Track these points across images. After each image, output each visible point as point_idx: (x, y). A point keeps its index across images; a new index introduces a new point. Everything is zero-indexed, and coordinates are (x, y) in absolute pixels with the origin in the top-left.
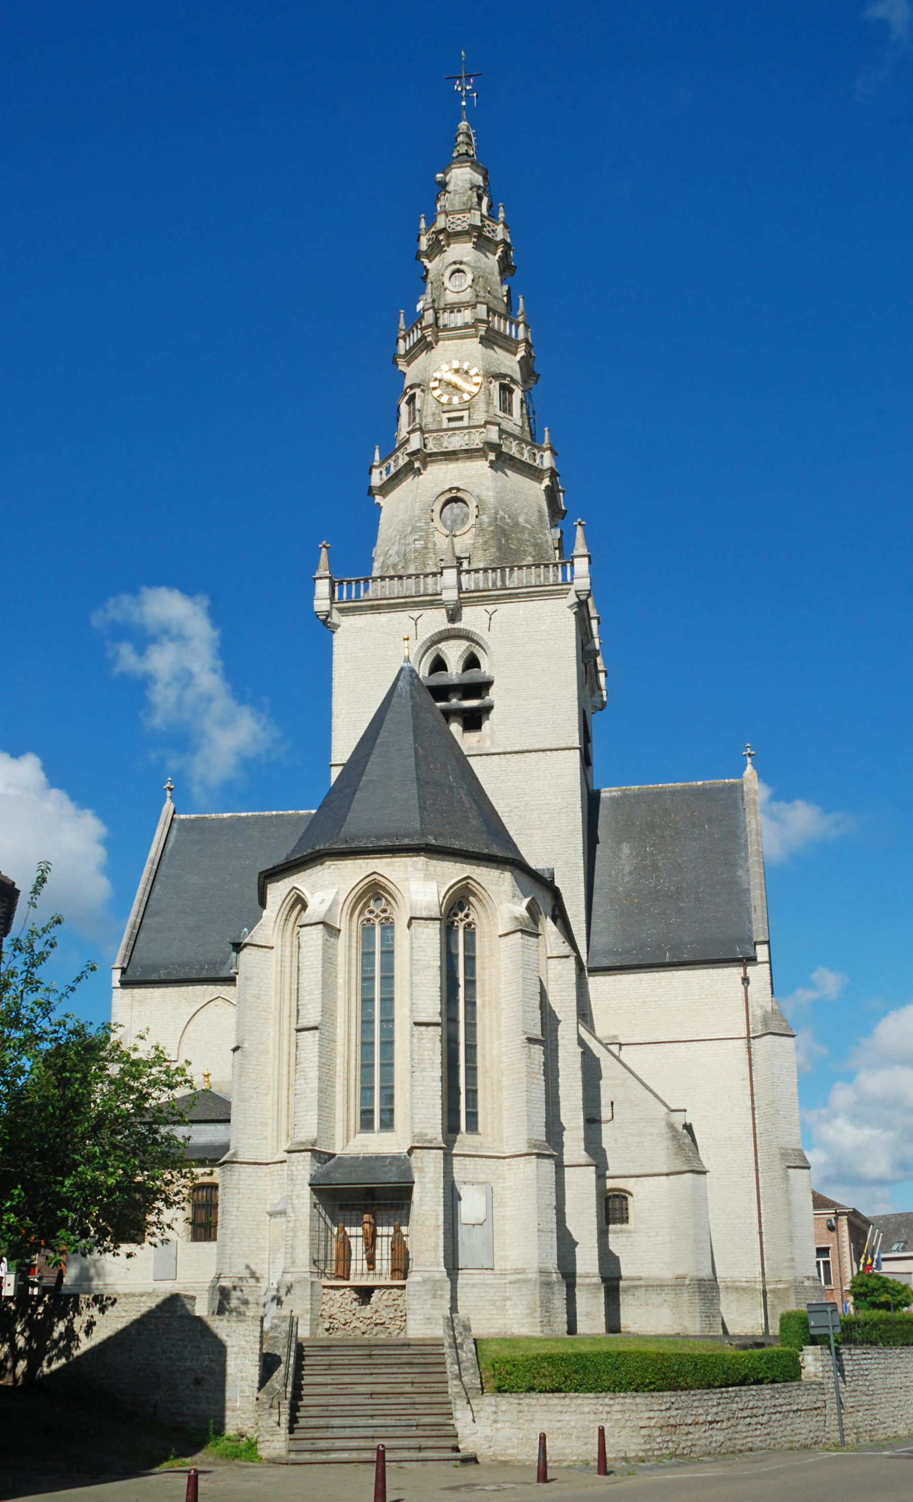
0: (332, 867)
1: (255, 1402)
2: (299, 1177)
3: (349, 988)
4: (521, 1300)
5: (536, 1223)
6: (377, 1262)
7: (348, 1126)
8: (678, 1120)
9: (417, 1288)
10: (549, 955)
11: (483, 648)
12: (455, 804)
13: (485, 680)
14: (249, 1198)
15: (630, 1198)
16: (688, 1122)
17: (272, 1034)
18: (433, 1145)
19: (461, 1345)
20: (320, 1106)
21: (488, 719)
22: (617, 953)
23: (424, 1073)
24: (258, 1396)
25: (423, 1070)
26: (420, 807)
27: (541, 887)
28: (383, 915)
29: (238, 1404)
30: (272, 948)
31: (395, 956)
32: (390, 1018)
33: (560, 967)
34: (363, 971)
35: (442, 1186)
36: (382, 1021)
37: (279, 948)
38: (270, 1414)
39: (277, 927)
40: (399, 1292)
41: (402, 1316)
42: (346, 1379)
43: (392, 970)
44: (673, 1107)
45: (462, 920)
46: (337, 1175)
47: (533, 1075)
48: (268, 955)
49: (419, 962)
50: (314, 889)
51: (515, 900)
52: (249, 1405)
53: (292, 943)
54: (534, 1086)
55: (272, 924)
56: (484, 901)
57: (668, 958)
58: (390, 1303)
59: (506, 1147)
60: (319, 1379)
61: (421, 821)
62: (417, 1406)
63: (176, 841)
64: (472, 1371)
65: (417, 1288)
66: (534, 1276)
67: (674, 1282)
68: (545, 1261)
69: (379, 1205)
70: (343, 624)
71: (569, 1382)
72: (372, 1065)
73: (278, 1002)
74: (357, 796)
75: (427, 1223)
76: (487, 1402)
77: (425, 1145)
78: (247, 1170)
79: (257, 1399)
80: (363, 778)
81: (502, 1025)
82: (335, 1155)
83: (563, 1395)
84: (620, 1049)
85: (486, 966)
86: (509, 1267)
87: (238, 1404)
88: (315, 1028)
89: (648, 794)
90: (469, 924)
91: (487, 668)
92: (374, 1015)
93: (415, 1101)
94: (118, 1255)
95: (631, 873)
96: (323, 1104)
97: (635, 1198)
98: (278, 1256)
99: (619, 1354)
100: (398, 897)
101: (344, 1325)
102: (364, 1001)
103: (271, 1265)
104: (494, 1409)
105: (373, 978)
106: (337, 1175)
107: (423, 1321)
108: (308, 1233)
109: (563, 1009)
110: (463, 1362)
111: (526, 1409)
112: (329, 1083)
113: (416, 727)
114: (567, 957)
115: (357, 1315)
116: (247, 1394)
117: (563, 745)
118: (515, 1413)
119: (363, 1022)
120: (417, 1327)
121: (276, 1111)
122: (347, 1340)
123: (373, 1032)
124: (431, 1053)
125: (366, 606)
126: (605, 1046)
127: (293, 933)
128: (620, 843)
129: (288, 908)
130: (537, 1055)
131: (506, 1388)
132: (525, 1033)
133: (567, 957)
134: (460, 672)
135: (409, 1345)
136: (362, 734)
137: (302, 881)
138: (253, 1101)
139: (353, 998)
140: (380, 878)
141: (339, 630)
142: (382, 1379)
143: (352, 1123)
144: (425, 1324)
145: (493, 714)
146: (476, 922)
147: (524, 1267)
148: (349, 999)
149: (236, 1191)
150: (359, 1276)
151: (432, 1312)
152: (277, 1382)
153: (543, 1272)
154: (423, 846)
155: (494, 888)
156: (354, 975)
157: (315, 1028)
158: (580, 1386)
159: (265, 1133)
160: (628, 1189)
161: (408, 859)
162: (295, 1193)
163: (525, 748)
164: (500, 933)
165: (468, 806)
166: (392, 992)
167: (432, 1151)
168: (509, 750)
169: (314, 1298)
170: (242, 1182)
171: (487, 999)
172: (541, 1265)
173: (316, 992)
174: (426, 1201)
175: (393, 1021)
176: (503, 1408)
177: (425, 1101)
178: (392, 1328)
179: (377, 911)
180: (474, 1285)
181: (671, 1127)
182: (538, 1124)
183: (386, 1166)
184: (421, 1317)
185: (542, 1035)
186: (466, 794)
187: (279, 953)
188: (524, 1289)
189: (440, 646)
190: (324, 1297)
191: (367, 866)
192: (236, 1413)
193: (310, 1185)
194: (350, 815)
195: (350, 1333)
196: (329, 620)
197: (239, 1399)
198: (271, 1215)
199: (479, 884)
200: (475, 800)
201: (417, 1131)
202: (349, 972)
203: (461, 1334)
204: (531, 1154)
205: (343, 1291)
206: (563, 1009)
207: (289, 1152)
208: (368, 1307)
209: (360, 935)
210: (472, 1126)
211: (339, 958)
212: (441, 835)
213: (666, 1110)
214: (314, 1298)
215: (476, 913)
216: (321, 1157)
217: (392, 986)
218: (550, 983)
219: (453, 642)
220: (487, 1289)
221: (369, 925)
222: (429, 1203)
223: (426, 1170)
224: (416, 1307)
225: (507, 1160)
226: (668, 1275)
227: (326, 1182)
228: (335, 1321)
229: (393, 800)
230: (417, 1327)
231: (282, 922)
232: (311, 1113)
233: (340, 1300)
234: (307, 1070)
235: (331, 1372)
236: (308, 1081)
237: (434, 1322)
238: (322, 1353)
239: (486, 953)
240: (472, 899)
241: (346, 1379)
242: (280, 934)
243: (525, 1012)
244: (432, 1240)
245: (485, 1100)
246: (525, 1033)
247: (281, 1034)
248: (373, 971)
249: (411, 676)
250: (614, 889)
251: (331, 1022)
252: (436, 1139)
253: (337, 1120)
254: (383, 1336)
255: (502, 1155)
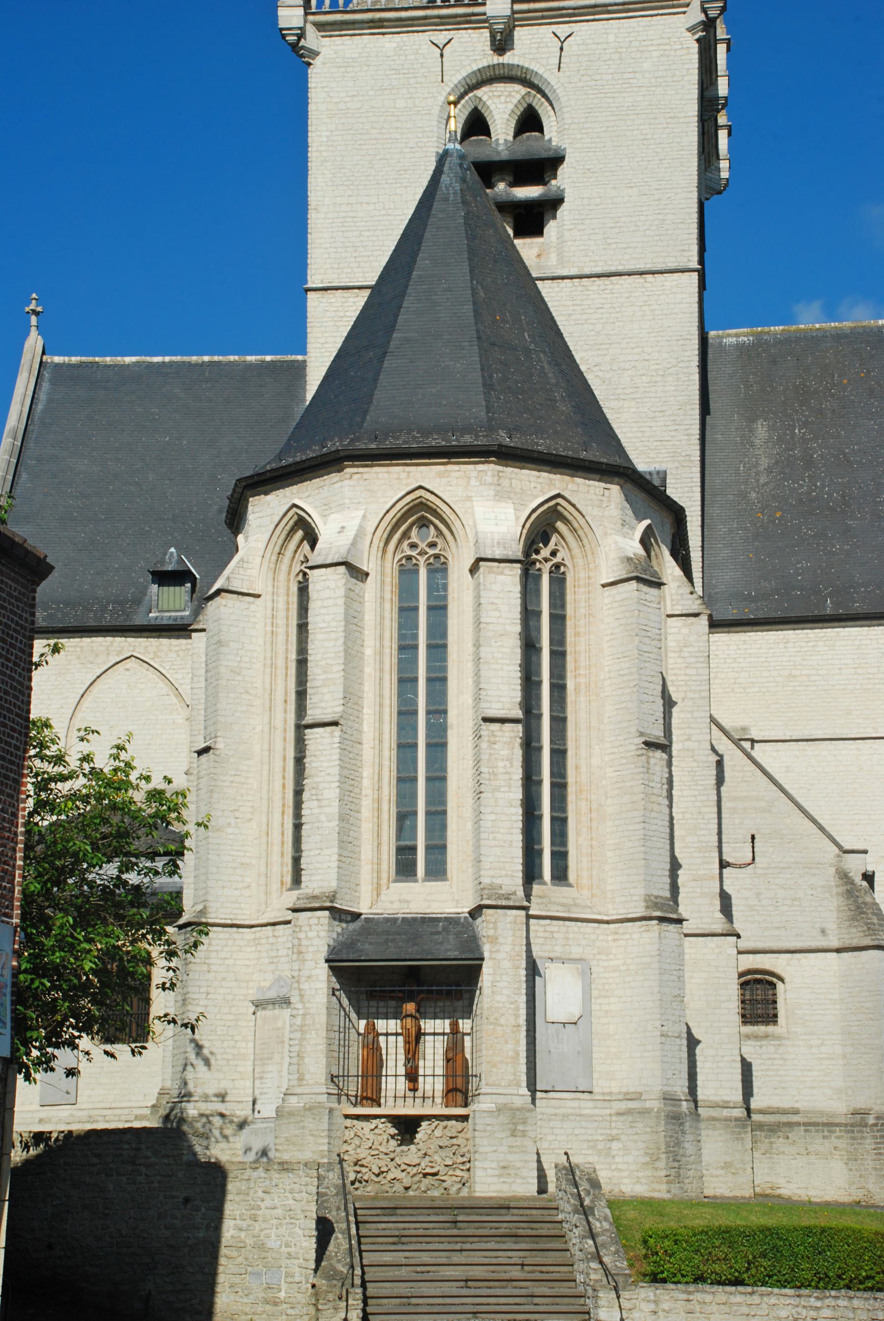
0: (356, 477)
1: (310, 1290)
2: (311, 949)
3: (381, 662)
4: (636, 1141)
5: (658, 1024)
6: (421, 1079)
7: (379, 872)
8: (855, 866)
9: (489, 1121)
10: (669, 613)
11: (551, 105)
12: (535, 379)
13: (551, 154)
14: (224, 979)
15: (779, 985)
16: (870, 869)
17: (259, 729)
18: (511, 903)
19: (592, 1209)
20: (341, 841)
21: (554, 217)
22: (749, 598)
23: (499, 795)
24: (315, 1282)
25: (497, 789)
26: (484, 385)
27: (647, 492)
28: (431, 552)
29: (282, 1295)
30: (259, 596)
31: (450, 615)
32: (442, 708)
33: (685, 631)
34: (401, 637)
35: (524, 965)
36: (428, 712)
37: (269, 598)
38: (336, 1309)
39: (266, 564)
40: (459, 1125)
41: (463, 1163)
42: (426, 1258)
43: (444, 635)
44: (847, 847)
45: (546, 560)
46: (367, 946)
47: (653, 798)
48: (253, 607)
49: (491, 627)
50: (327, 509)
51: (625, 529)
52: (299, 1296)
53: (288, 588)
54: (653, 815)
55: (260, 559)
56: (580, 532)
57: (829, 608)
58: (444, 1142)
59: (610, 906)
60: (387, 1258)
61: (487, 407)
62: (536, 1300)
63: (50, 400)
64: (613, 1249)
65: (489, 1121)
66: (655, 1105)
67: (849, 1120)
68: (670, 1081)
69: (430, 992)
70: (324, 51)
71: (753, 1271)
72: (415, 779)
73: (268, 680)
74: (386, 364)
75: (503, 1021)
76: (643, 1296)
77: (499, 903)
78: (221, 936)
79: (313, 1286)
80: (394, 335)
81: (606, 721)
82: (361, 914)
83: (749, 1289)
84: (752, 748)
85: (582, 630)
86: (615, 1090)
87: (282, 1295)
88: (335, 724)
89: (798, 340)
90: (557, 566)
91: (554, 132)
92: (416, 704)
93: (483, 836)
94: (52, 1070)
95: (769, 470)
96: (345, 838)
97: (788, 985)
98: (269, 1068)
99: (823, 1230)
100: (456, 526)
101: (378, 1175)
102: (401, 681)
103: (257, 1083)
104: (652, 1307)
105: (416, 647)
106: (367, 946)
107: (498, 1172)
108: (324, 1034)
109: (690, 695)
110: (598, 1235)
111: (698, 1308)
112: (353, 807)
113: (472, 253)
114: (696, 615)
115: (398, 1160)
116: (297, 1279)
117: (672, 265)
118: (683, 1313)
119: (400, 713)
120: (489, 1180)
121: (264, 847)
122: (385, 1198)
123: (415, 728)
124: (508, 764)
125: (362, 22)
126: (737, 742)
127: (289, 574)
128: (752, 420)
129: (283, 536)
130: (658, 768)
131: (665, 1275)
132: (642, 734)
133: (696, 615)
134: (511, 138)
135: (508, 1208)
136: (386, 259)
137: (308, 496)
138: (230, 830)
139: (387, 677)
140: (428, 496)
141: (317, 62)
142: (477, 1258)
143: (385, 867)
144: (500, 1176)
145: (563, 212)
146: (566, 562)
147: (639, 1089)
148: (381, 679)
149: (205, 968)
150: (395, 1097)
151: (510, 1157)
152: (339, 1261)
153: (669, 1098)
154: (495, 448)
155: (595, 512)
156: (387, 643)
157: (335, 724)
158: (770, 1277)
159: (248, 880)
160: (778, 971)
161: (471, 467)
162: (305, 973)
163: (613, 269)
164: (603, 582)
165: (553, 381)
166: (444, 669)
167: (509, 912)
168: (587, 271)
169: (333, 1134)
170: (213, 955)
171: (582, 680)
172: (666, 1088)
173: (335, 669)
174: (499, 983)
175: (445, 712)
176: (666, 1306)
177: (499, 836)
178: (449, 1181)
179: (423, 545)
180: (565, 1117)
181: (844, 876)
182: (659, 872)
183: (438, 933)
184: (494, 1165)
185: (665, 737)
186: (549, 363)
187: (269, 604)
188: (640, 1125)
189: (479, 93)
190: (347, 1132)
191: (408, 477)
192: (280, 1308)
193: (327, 961)
194: (377, 394)
195: (386, 1188)
196: (302, 43)
197: (284, 1286)
198: (259, 1005)
199: (574, 506)
200: (562, 371)
201: (486, 881)
202: (381, 638)
203: (588, 1193)
204: (650, 918)
205: (375, 1122)
206: (690, 695)
207: (295, 910)
208: (412, 1147)
209: (396, 581)
210: (560, 875)
211: (366, 617)
212: (517, 429)
213: (836, 850)
214: (333, 1134)
215: (564, 547)
216: (337, 914)
217: (444, 659)
218: (670, 655)
219: (500, 87)
220: (584, 1124)
221: (409, 566)
222: (505, 991)
223: (501, 940)
224: (488, 1149)
225: (612, 926)
226: (839, 1107)
227: (351, 957)
228: (364, 1170)
229: (440, 372)
230: (489, 1180)
231: (274, 558)
232: (329, 852)
233: (371, 1136)
234: (321, 786)
235: (404, 1247)
236: (324, 803)
237: (512, 1172)
238: (386, 1219)
239: (582, 611)
240: (559, 525)
241: (426, 1258)
242: (271, 575)
243: (642, 702)
244: (510, 1047)
245: (578, 834)
246: (642, 734)
247: (271, 728)
248: (416, 636)
249: (461, 165)
250: (744, 495)
251: (356, 713)
252: (514, 893)
253: (363, 863)
254: (436, 1193)
255: (606, 918)
